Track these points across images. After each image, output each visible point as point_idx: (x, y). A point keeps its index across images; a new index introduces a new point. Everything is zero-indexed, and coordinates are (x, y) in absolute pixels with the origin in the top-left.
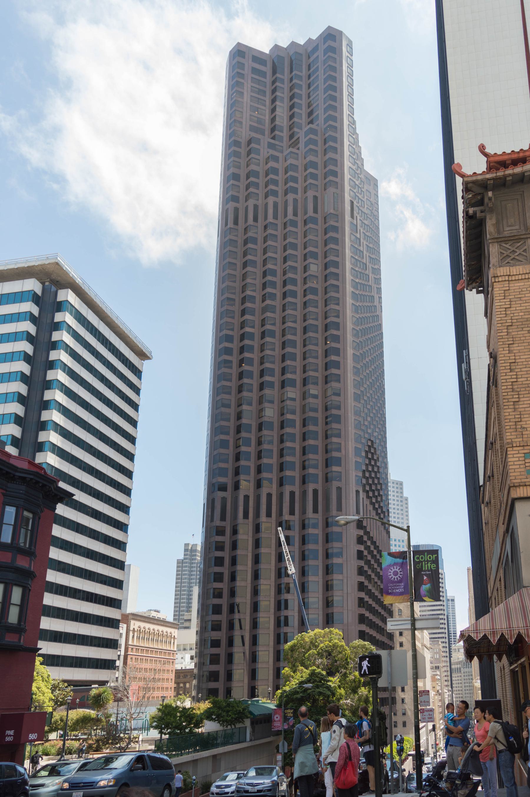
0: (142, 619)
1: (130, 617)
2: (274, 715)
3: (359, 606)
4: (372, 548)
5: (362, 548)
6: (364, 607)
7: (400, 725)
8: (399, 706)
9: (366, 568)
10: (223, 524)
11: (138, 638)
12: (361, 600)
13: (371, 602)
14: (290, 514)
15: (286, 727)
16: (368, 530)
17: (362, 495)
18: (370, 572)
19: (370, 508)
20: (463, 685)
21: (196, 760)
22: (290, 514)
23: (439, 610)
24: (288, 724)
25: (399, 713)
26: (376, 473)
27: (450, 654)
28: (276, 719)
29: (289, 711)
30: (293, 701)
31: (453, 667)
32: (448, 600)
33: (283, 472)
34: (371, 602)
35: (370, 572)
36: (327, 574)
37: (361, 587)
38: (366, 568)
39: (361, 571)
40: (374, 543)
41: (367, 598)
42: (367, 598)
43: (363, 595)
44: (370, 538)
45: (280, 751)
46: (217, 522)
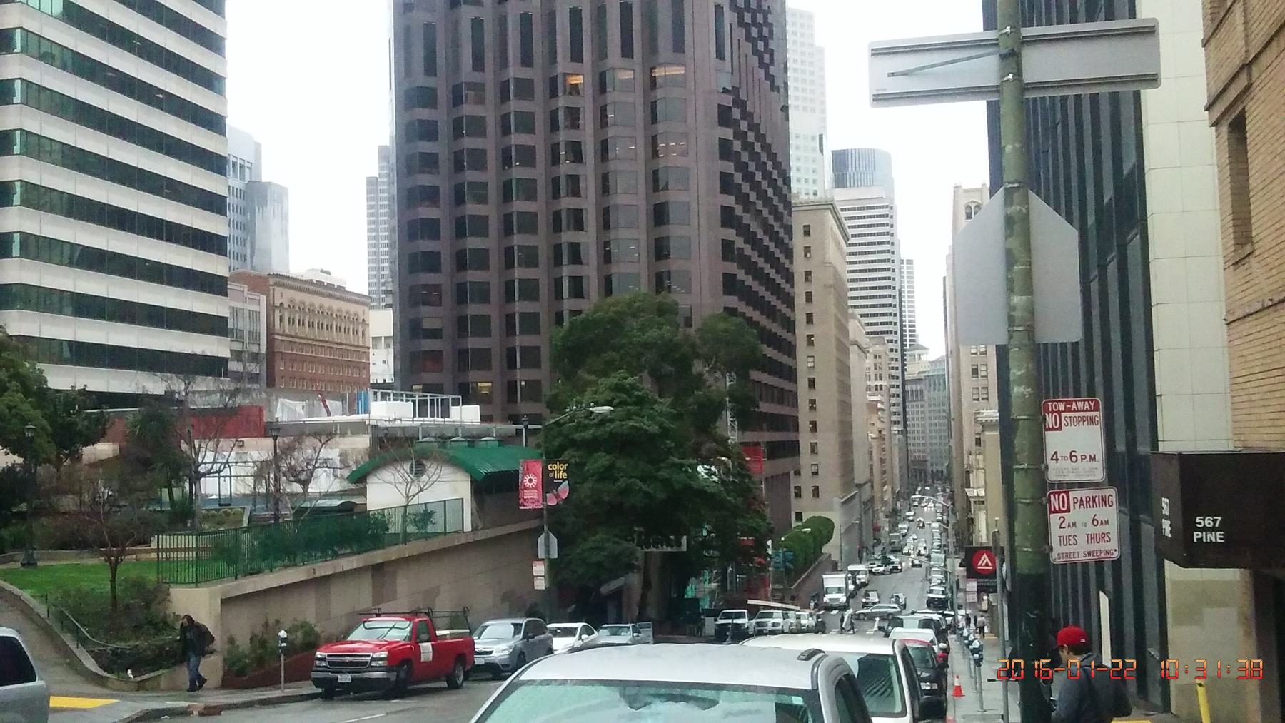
0: (298, 284)
1: (271, 282)
2: (524, 475)
3: (725, 258)
4: (751, 137)
5: (728, 133)
6: (732, 260)
7: (807, 493)
8: (805, 458)
9: (739, 210)
10: (430, 82)
11: (291, 321)
12: (727, 245)
13: (749, 281)
14: (572, 60)
15: (552, 502)
16: (743, 96)
17: (729, 17)
18: (746, 188)
19: (748, 47)
20: (928, 422)
21: (326, 579)
22: (572, 60)
23: (884, 279)
24: (557, 496)
25: (806, 473)
26: (760, 27)
27: (903, 365)
28: (528, 484)
29: (558, 466)
30: (574, 443)
31: (908, 388)
32: (902, 262)
33: (664, 227)
34: (749, 281)
35: (746, 188)
36: (656, 190)
37: (728, 218)
38: (739, 210)
39: (726, 184)
40: (754, 127)
41: (739, 242)
42: (739, 242)
43: (731, 234)
44: (746, 115)
45: (541, 555)
46: (422, 80)
